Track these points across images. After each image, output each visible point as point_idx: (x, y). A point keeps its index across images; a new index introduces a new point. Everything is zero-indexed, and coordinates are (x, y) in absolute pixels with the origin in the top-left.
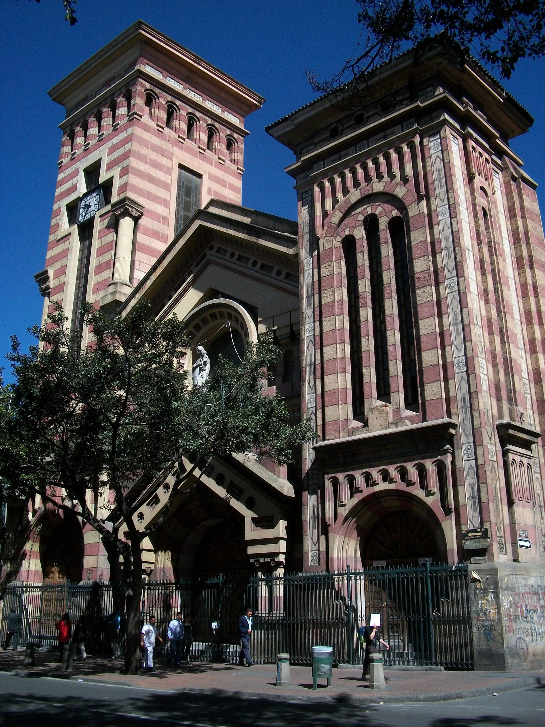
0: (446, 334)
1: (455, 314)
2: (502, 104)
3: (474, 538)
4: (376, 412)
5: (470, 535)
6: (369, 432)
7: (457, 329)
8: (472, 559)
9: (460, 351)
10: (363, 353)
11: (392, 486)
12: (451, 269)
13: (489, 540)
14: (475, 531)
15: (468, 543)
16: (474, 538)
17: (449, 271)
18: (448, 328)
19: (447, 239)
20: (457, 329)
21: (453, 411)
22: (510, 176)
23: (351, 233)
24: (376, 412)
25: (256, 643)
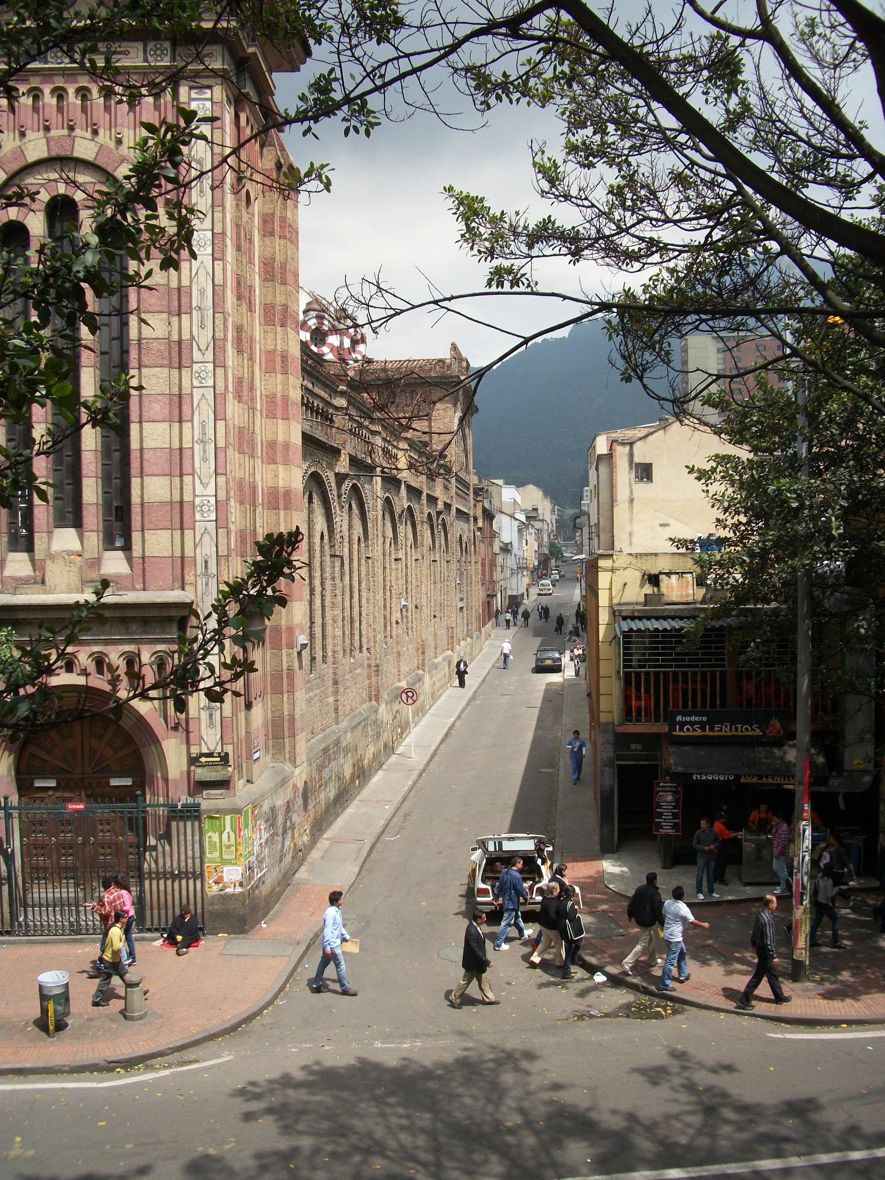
0: (187, 454)
1: (203, 424)
2: (710, 929)
3: (208, 764)
4: (60, 562)
5: (203, 759)
6: (46, 593)
7: (205, 451)
8: (205, 792)
9: (205, 488)
10: (539, 705)
11: (81, 681)
12: (203, 348)
13: (230, 769)
14: (210, 755)
15: (199, 771)
16: (208, 764)
17: (199, 349)
18: (190, 445)
19: (202, 292)
20: (205, 451)
21: (189, 578)
22: (274, 161)
23: (20, 219)
24: (60, 562)
25: (182, 837)
